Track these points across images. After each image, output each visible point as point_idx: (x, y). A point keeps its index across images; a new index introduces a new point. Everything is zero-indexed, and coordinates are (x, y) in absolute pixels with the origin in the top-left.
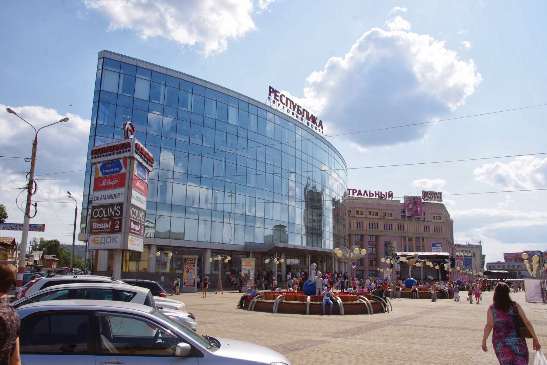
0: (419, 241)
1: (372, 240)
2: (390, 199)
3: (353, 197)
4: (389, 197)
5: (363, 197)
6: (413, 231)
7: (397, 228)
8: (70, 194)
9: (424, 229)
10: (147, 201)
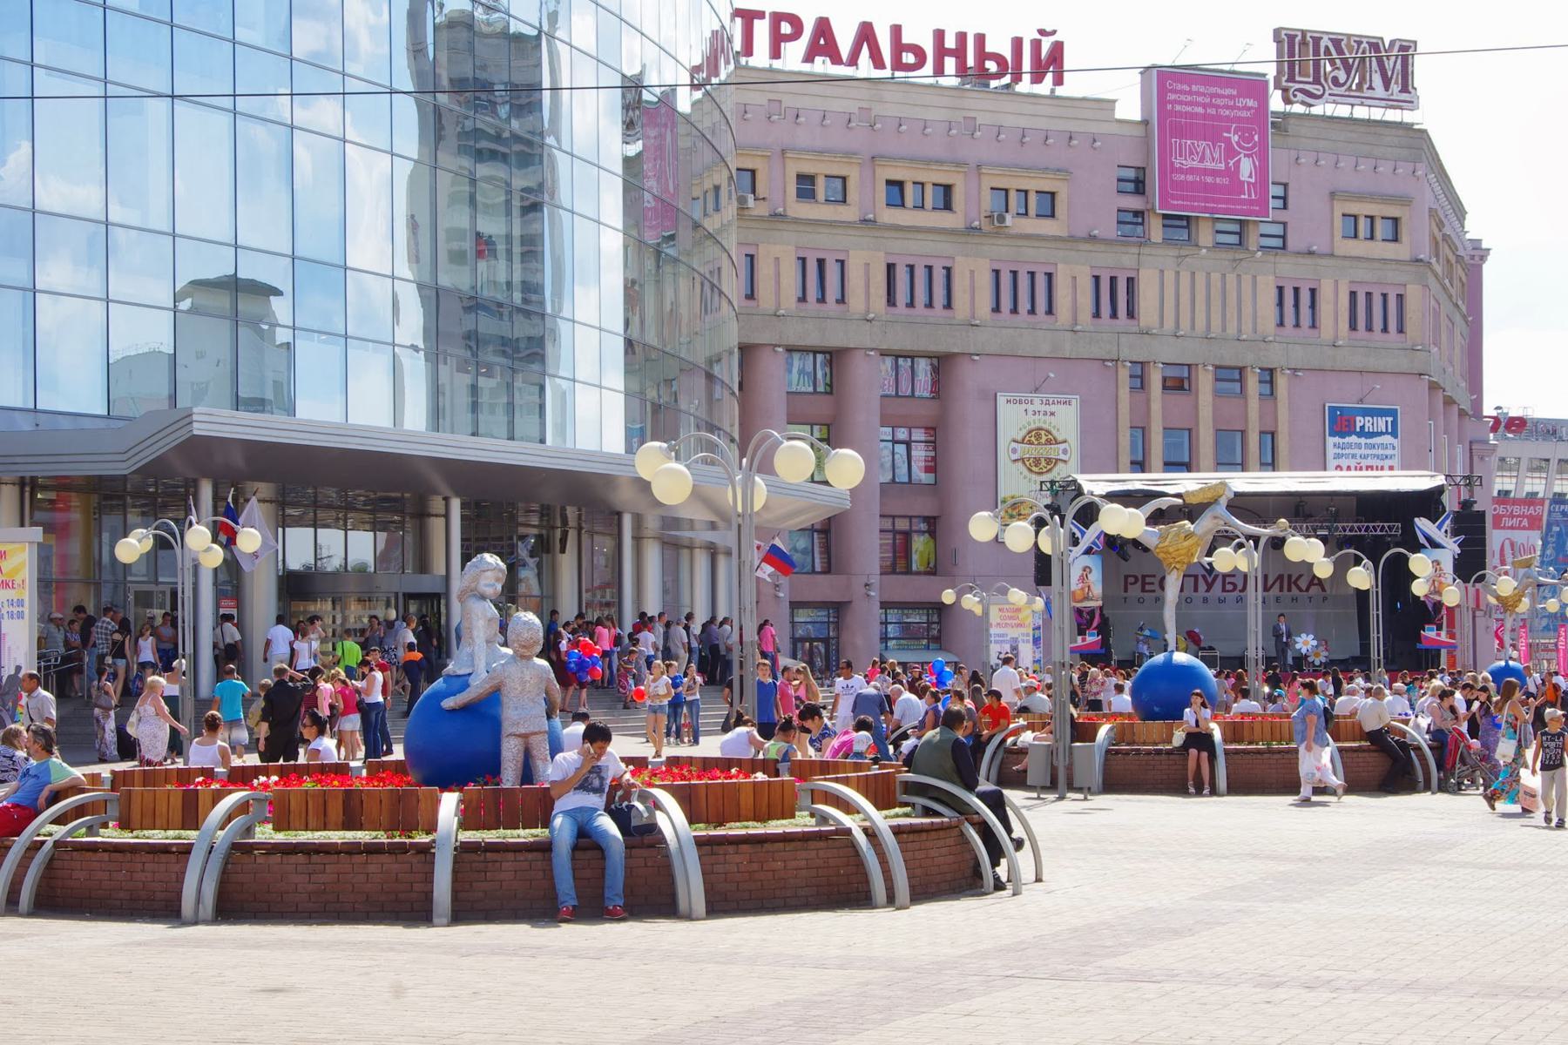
7: (1087, 302)
9: (1281, 303)
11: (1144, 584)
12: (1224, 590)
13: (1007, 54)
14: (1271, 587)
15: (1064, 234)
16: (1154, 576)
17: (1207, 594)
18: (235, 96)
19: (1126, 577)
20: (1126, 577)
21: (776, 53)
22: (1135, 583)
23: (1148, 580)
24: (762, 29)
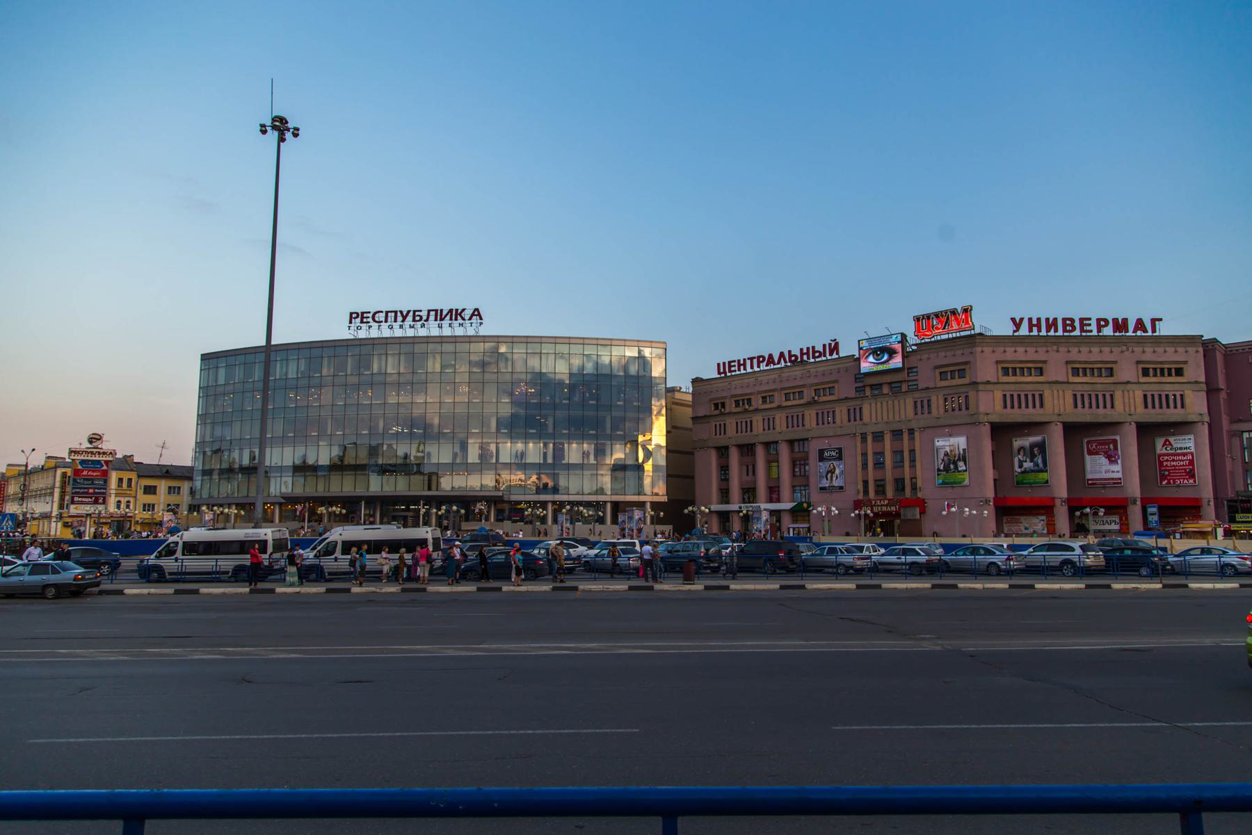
0: (902, 440)
1: (801, 450)
2: (835, 356)
3: (1029, 336)
4: (831, 354)
5: (779, 366)
6: (885, 418)
7: (845, 417)
8: (1032, 545)
9: (916, 407)
10: (894, 452)
11: (363, 318)
12: (414, 320)
13: (822, 350)
15: (836, 398)
19: (351, 314)
20: (351, 314)
21: (759, 367)
22: (357, 317)
23: (365, 315)
24: (755, 361)
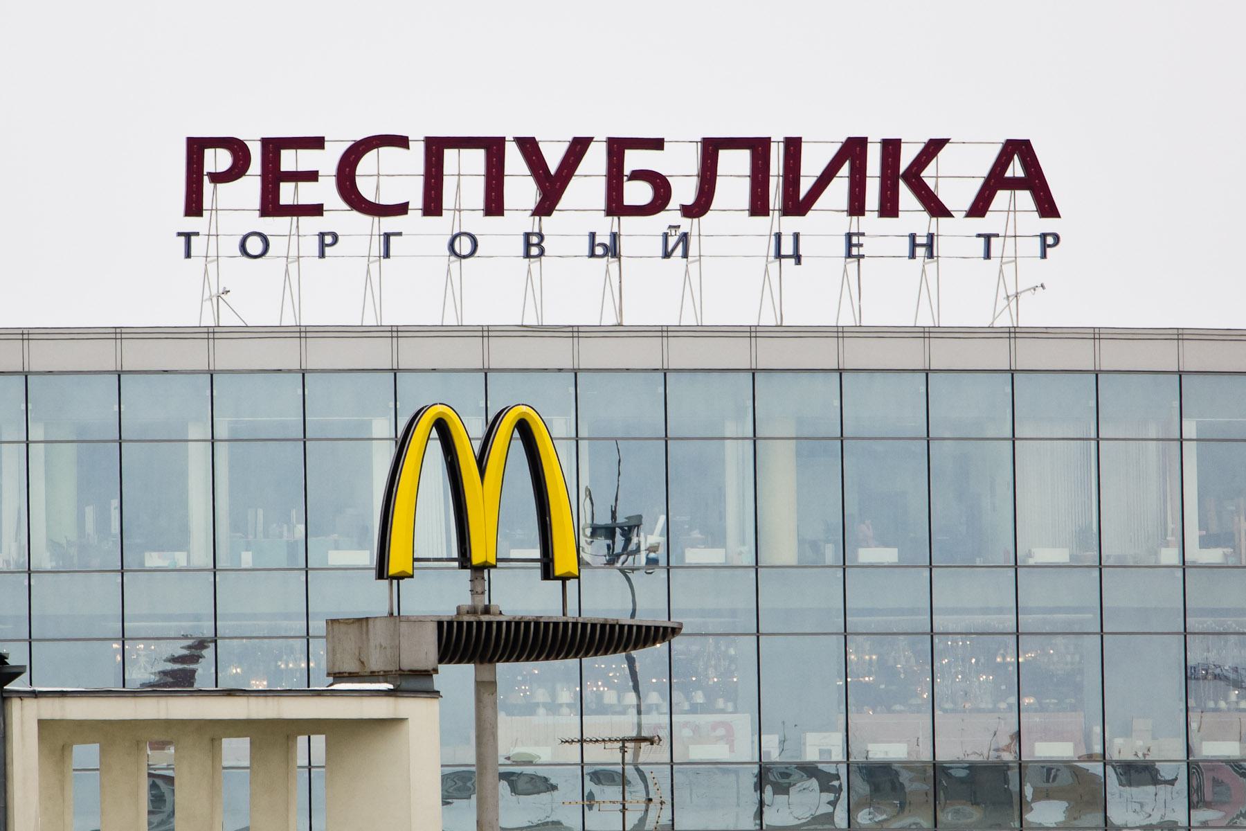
11: (273, 177)
12: (616, 206)
14: (673, 250)
16: (317, 143)
17: (686, 224)
18: (1015, 236)
19: (196, 148)
20: (196, 148)
22: (238, 170)
